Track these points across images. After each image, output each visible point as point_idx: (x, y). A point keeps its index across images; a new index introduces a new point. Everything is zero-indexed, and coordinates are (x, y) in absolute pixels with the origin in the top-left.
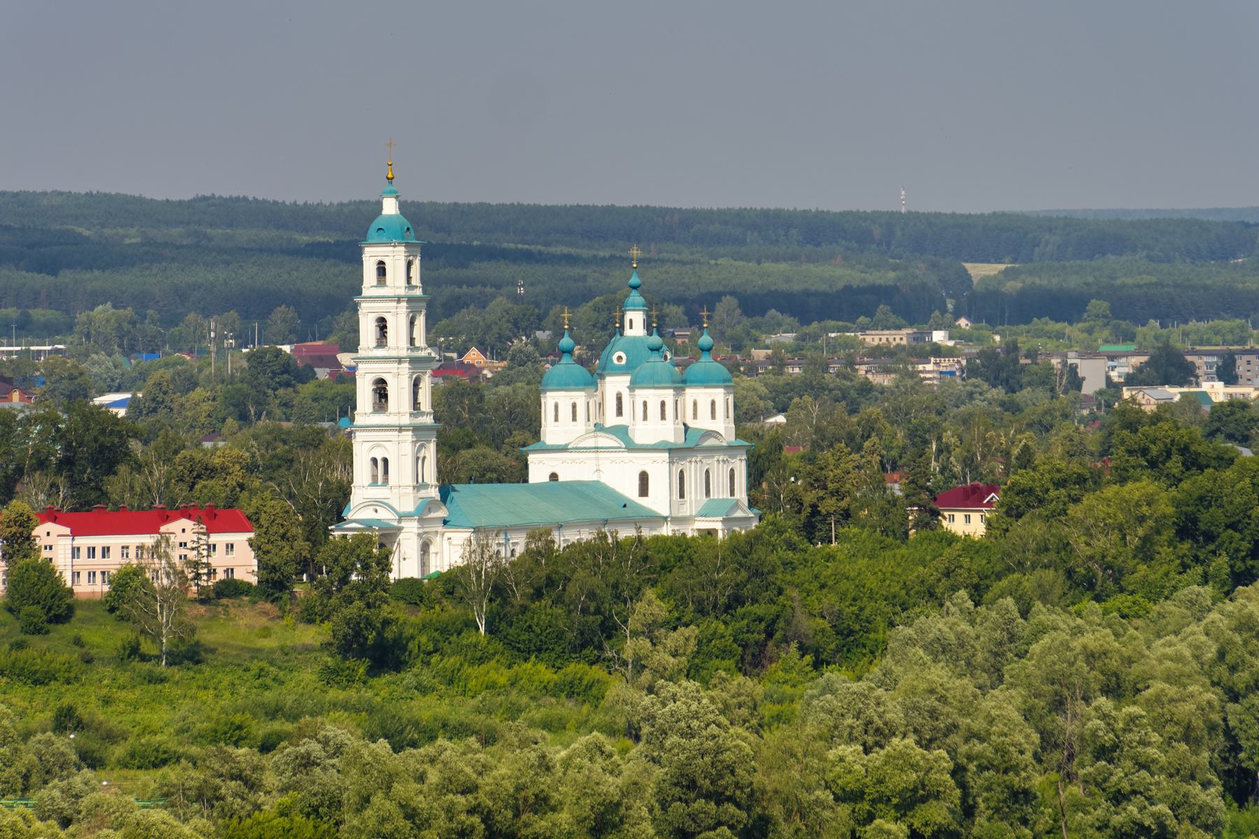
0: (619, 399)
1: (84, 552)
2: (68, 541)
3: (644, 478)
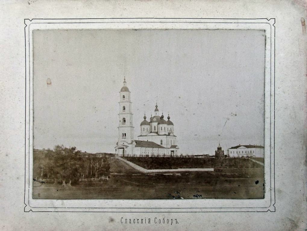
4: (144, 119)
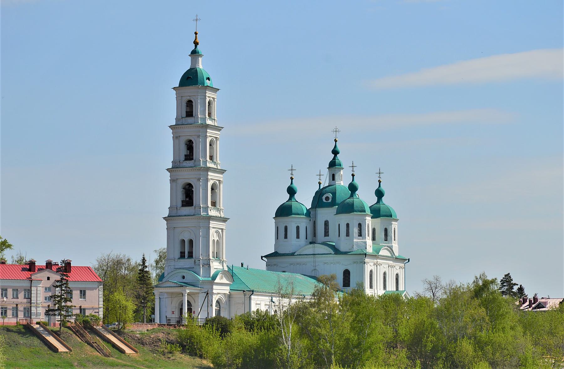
0: (326, 223)
4: (375, 199)
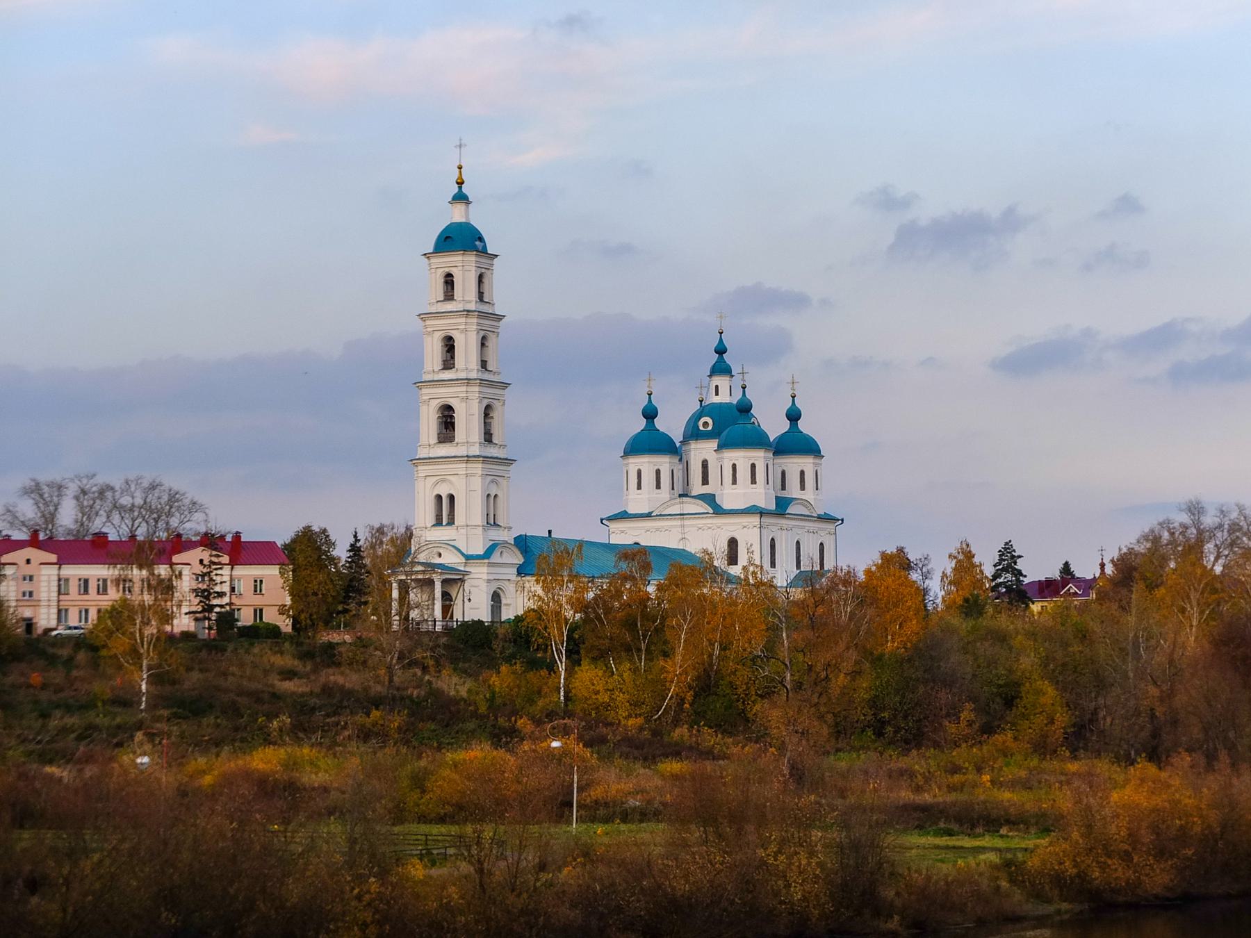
0: (705, 465)
1: (74, 587)
2: (53, 570)
3: (733, 543)
